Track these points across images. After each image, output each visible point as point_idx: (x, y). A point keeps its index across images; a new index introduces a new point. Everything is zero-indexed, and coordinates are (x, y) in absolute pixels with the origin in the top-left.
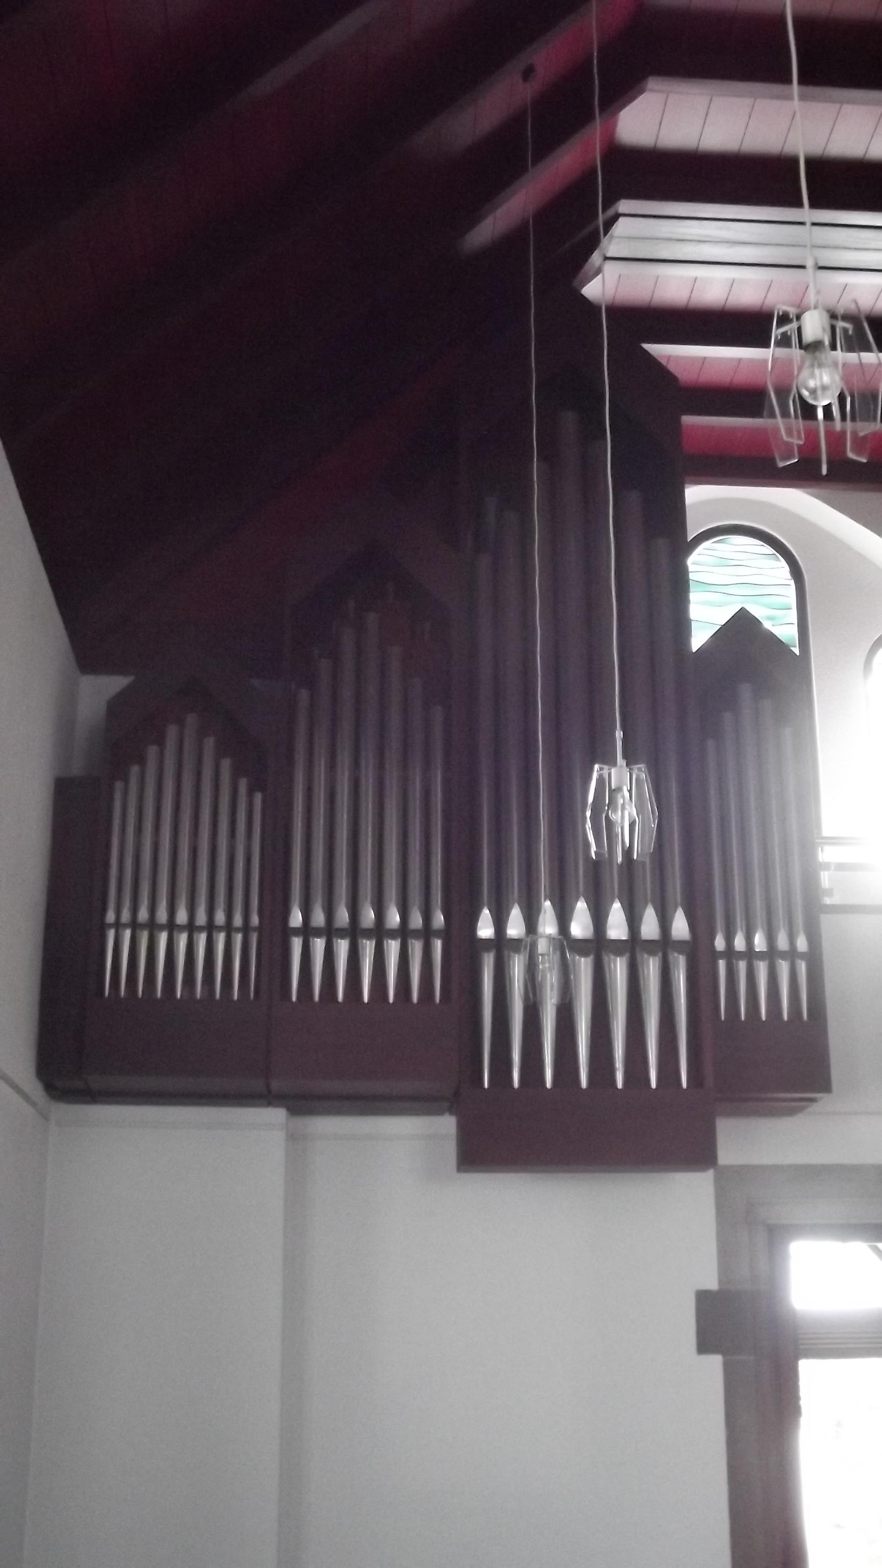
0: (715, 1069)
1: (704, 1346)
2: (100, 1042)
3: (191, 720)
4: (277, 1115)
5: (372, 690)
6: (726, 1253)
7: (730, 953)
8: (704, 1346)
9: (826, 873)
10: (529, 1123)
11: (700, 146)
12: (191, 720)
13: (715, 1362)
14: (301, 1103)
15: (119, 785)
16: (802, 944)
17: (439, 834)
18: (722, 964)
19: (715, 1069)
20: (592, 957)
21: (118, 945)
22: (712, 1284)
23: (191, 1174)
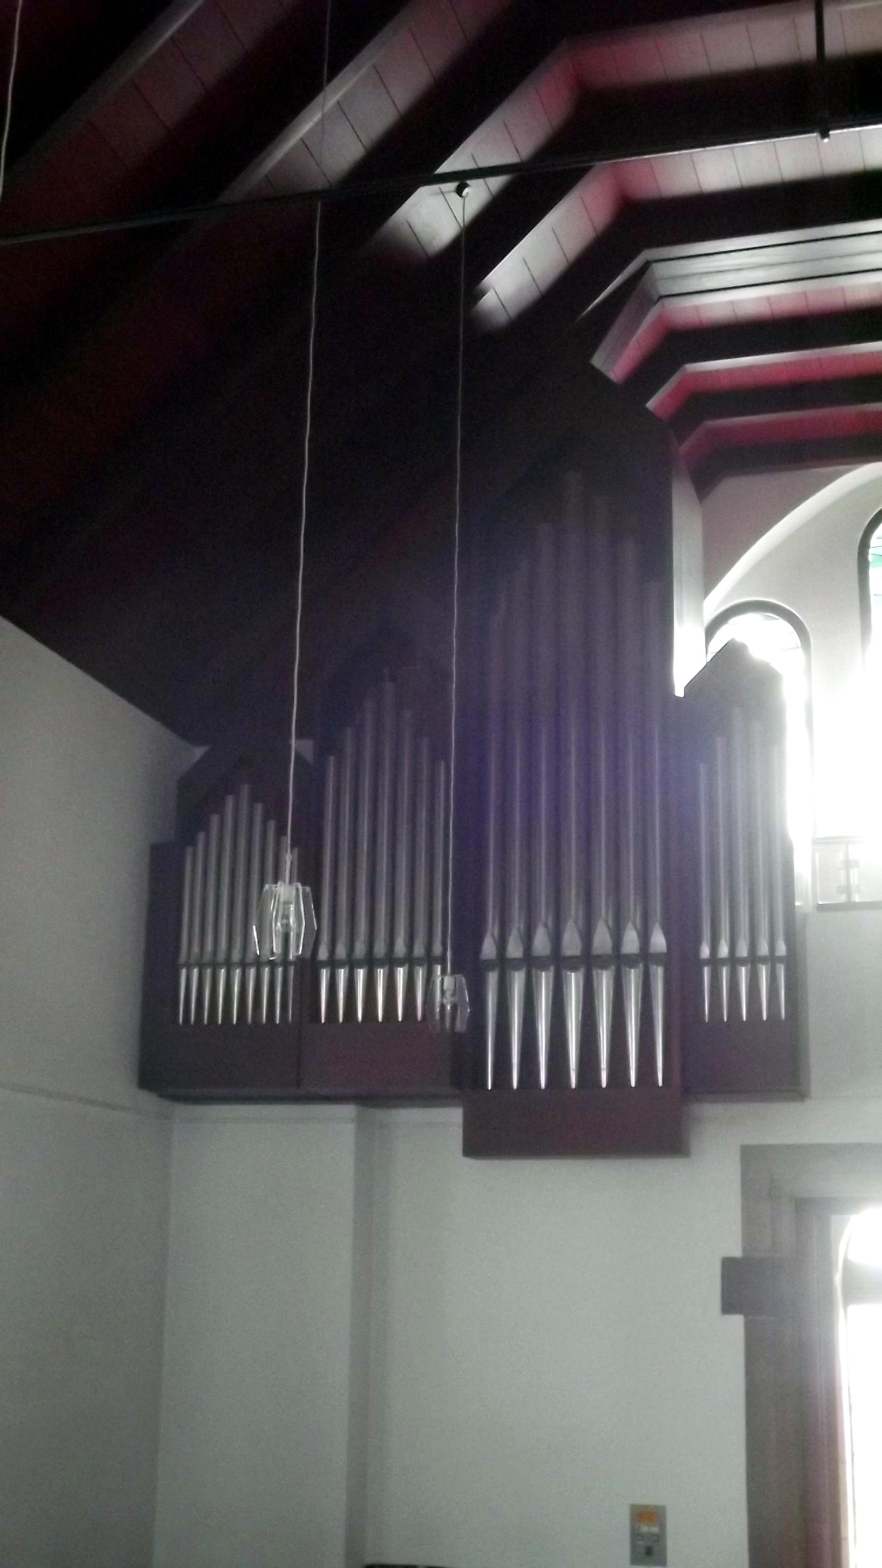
0: (719, 1059)
1: (728, 1307)
2: (189, 1058)
3: (245, 789)
4: (348, 1111)
5: (387, 753)
6: (750, 1222)
7: (715, 962)
8: (728, 1307)
9: (856, 870)
10: (527, 1122)
11: (536, 274)
12: (245, 789)
13: (737, 1322)
14: (369, 1098)
15: (189, 850)
16: (782, 949)
17: (384, 888)
18: (706, 971)
19: (719, 1059)
20: (582, 970)
21: (189, 980)
22: (737, 1252)
23: (275, 1164)
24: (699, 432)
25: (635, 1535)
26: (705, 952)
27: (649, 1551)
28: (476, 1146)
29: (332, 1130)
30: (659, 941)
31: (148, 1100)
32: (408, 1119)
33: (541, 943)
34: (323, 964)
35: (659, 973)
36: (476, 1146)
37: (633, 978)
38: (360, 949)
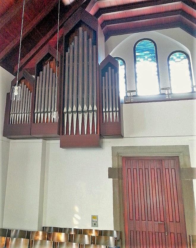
1: (109, 177)
4: (41, 140)
8: (109, 177)
10: (71, 141)
12: (23, 83)
14: (45, 138)
21: (12, 116)
24: (106, 27)
25: (92, 221)
26: (104, 110)
27: (95, 224)
28: (62, 146)
29: (36, 144)
30: (95, 108)
31: (5, 138)
32: (52, 142)
33: (75, 109)
34: (36, 113)
35: (95, 113)
36: (62, 146)
37: (91, 115)
38: (42, 110)
